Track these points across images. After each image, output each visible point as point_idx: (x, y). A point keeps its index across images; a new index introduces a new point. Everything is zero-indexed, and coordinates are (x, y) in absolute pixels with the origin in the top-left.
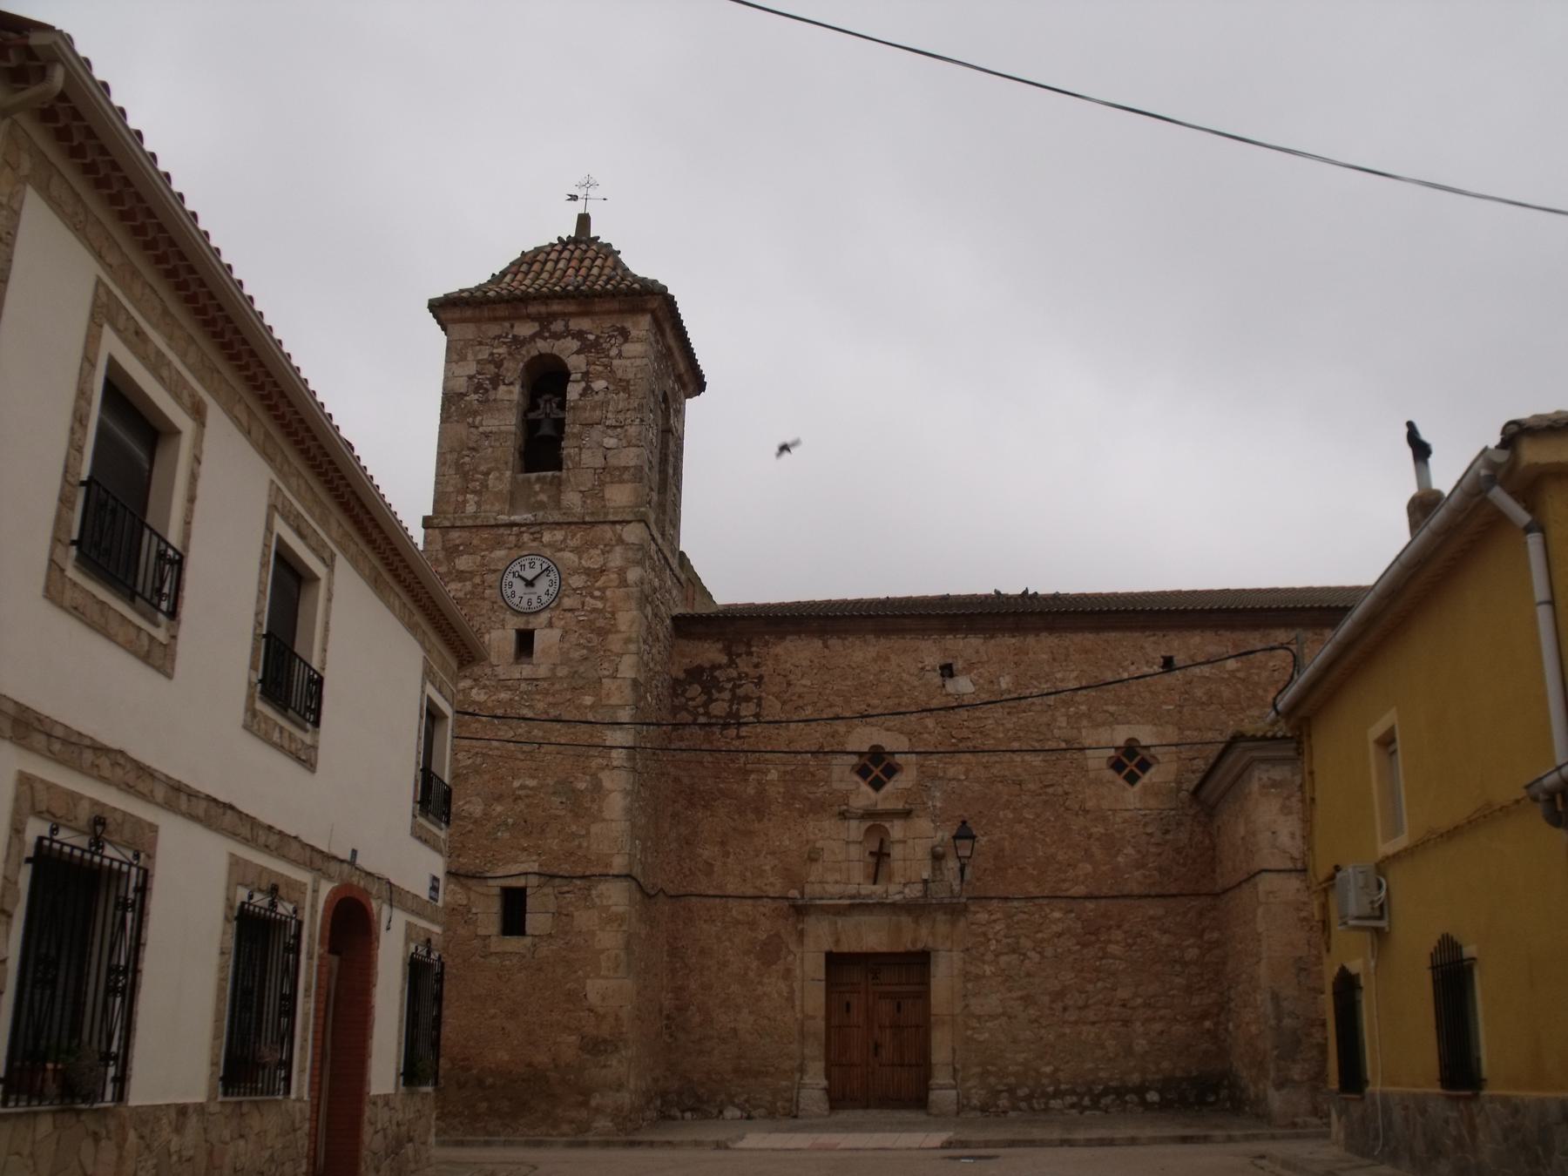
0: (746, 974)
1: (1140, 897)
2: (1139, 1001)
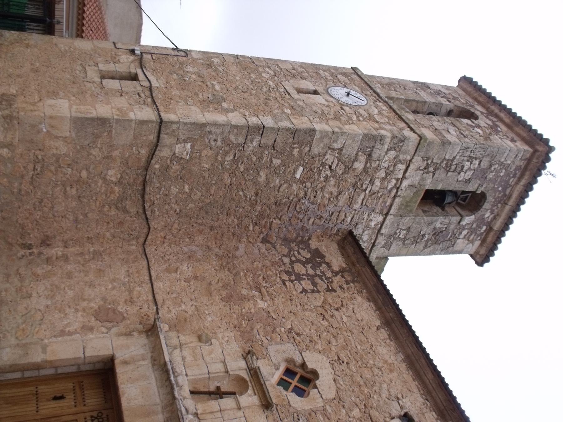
0: (84, 300)
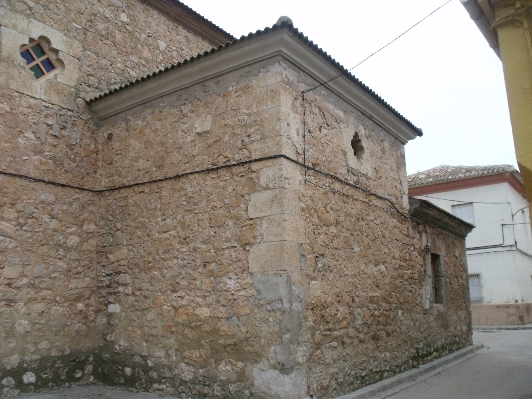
1: (36, 180)
2: (25, 281)
